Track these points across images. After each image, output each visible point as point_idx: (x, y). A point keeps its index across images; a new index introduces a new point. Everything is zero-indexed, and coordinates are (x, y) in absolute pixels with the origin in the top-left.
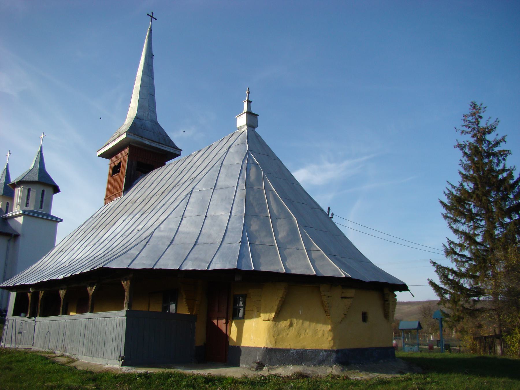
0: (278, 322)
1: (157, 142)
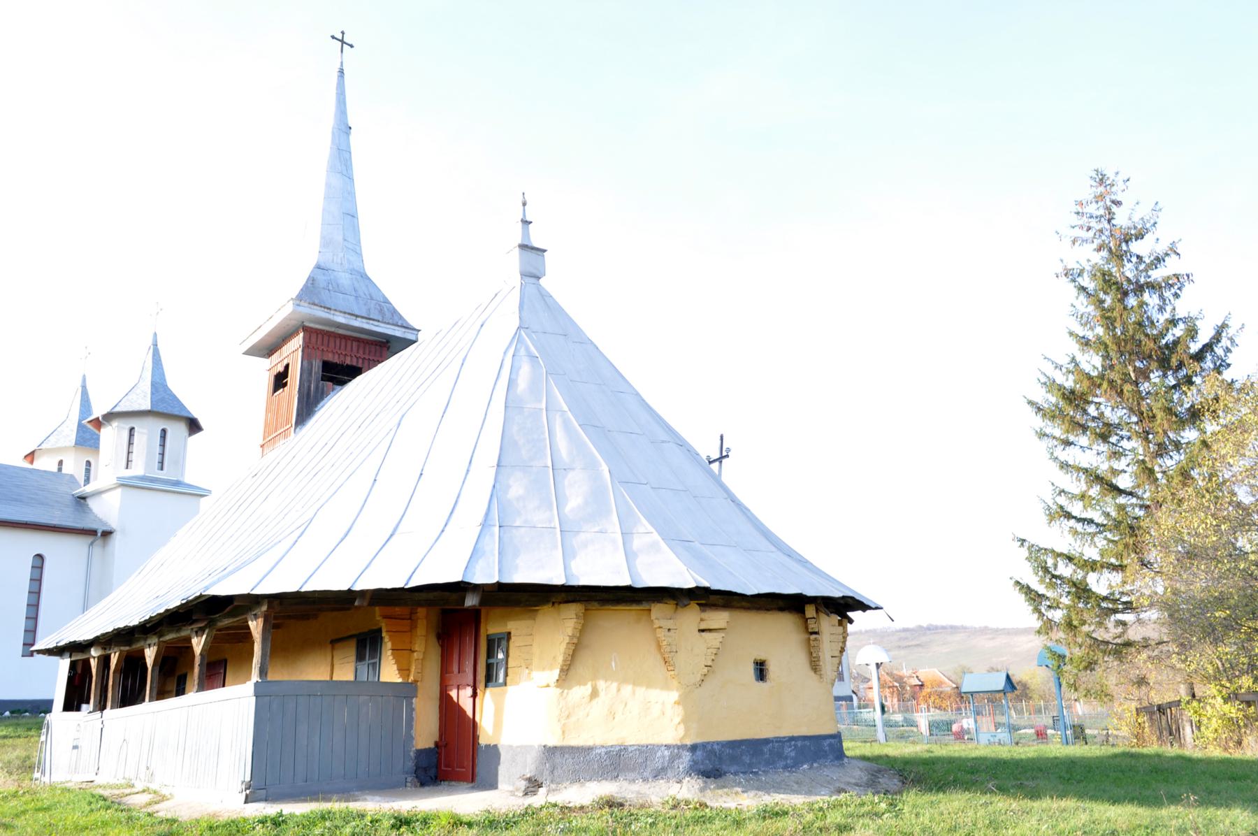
0: (568, 689)
1: (363, 317)
